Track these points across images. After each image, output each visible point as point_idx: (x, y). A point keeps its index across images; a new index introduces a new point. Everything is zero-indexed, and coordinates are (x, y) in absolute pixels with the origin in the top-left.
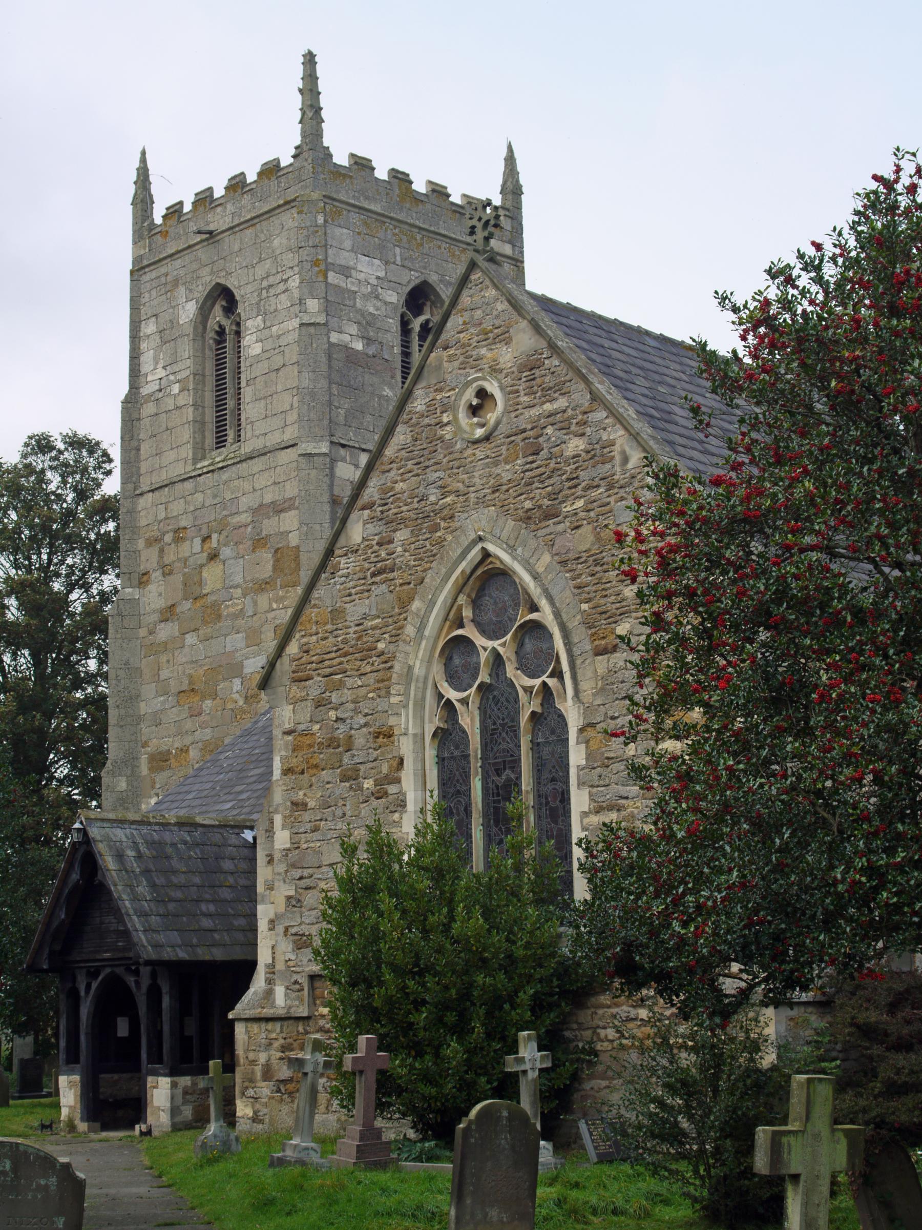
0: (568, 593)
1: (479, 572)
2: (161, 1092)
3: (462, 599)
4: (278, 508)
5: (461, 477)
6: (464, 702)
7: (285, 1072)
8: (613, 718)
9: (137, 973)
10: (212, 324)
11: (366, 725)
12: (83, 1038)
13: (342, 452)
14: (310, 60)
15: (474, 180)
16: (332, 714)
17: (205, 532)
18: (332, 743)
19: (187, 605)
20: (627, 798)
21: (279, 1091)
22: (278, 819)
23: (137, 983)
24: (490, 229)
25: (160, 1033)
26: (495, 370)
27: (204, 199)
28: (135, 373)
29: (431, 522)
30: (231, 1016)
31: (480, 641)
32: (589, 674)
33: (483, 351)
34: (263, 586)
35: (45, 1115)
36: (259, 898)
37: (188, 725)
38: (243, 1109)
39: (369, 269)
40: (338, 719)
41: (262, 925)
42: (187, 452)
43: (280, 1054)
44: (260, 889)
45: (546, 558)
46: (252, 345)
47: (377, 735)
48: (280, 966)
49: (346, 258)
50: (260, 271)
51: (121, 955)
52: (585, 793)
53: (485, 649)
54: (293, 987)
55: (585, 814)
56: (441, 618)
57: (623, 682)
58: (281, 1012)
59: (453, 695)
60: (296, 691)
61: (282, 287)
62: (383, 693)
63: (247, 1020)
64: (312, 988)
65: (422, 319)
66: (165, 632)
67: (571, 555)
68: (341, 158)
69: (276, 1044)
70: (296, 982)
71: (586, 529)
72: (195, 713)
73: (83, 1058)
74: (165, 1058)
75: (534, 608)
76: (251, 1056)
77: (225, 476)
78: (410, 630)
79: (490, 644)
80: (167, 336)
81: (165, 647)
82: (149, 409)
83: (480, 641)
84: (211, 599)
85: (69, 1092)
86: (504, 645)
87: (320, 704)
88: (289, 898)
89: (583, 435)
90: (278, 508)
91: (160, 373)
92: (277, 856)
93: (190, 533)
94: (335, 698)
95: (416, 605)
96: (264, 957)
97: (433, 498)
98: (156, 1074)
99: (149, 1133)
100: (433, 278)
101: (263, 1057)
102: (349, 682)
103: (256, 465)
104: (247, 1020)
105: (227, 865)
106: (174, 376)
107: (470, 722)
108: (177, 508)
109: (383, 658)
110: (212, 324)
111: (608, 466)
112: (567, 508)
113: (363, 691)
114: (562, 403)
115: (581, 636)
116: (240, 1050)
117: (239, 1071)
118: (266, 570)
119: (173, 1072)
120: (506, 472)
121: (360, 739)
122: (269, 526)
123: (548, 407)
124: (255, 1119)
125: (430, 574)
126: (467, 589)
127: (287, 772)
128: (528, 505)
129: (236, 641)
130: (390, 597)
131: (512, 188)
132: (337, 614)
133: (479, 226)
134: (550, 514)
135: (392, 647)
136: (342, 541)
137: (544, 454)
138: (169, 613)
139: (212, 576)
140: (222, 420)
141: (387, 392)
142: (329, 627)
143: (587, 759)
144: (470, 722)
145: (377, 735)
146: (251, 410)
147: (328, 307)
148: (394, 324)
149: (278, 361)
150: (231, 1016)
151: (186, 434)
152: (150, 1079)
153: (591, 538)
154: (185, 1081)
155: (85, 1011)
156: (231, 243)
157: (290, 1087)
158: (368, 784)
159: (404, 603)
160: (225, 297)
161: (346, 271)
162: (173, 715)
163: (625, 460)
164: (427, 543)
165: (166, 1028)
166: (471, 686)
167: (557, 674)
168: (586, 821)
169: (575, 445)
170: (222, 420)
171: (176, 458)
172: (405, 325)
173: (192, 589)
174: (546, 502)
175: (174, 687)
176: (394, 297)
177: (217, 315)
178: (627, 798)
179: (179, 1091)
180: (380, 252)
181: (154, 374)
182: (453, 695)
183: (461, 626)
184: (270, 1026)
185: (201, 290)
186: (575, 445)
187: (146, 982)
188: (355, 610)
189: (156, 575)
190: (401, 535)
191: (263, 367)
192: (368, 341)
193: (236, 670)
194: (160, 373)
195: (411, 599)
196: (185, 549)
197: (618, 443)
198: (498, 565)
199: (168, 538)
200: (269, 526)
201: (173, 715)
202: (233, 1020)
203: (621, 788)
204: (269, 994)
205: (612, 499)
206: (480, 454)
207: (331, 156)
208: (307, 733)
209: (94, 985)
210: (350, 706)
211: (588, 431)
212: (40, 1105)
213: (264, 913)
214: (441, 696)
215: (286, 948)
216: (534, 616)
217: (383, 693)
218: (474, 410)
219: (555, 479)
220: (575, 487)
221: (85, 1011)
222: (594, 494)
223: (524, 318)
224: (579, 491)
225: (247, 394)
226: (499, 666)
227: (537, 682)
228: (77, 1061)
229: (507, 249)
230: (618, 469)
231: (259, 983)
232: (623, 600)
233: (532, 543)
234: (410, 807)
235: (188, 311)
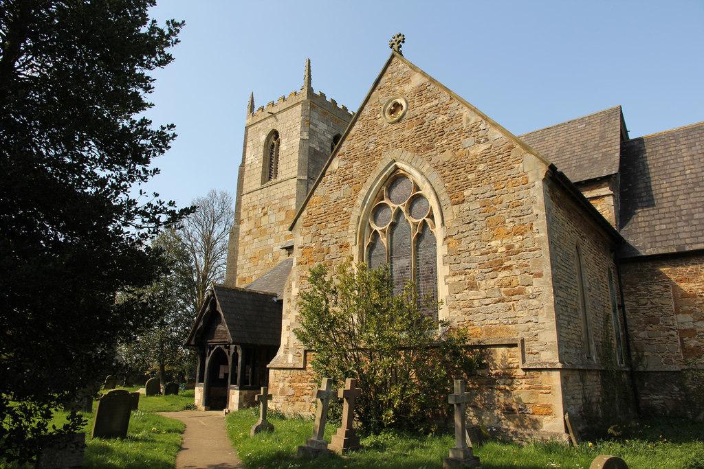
0: (438, 179)
1: (392, 176)
2: (235, 396)
3: (384, 189)
4: (288, 198)
5: (385, 138)
6: (383, 231)
7: (291, 392)
8: (462, 232)
9: (229, 348)
10: (271, 143)
11: (336, 242)
12: (206, 373)
16: (321, 239)
17: (263, 206)
18: (321, 251)
20: (470, 269)
21: (287, 400)
22: (294, 284)
23: (229, 352)
24: (401, 43)
25: (236, 375)
26: (402, 94)
30: (268, 366)
32: (450, 213)
35: (188, 401)
36: (283, 317)
39: (322, 127)
40: (323, 241)
43: (289, 384)
44: (284, 313)
45: (427, 166)
46: (283, 147)
47: (341, 247)
48: (291, 345)
49: (315, 121)
50: (288, 125)
51: (223, 340)
52: (447, 267)
53: (394, 208)
54: (297, 355)
55: (446, 277)
56: (374, 196)
57: (468, 216)
58: (291, 366)
62: (345, 229)
63: (275, 369)
64: (305, 356)
66: (248, 238)
67: (441, 163)
68: (317, 92)
69: (287, 379)
70: (298, 353)
73: (205, 380)
74: (238, 382)
76: (276, 384)
77: (271, 188)
79: (397, 206)
80: (254, 147)
84: (263, 228)
85: (199, 393)
88: (297, 316)
89: (446, 114)
90: (288, 198)
91: (252, 157)
92: (292, 299)
93: (258, 207)
96: (284, 341)
97: (372, 148)
98: (233, 389)
99: (229, 411)
101: (281, 385)
102: (329, 225)
104: (275, 369)
105: (267, 309)
106: (255, 158)
108: (254, 199)
109: (345, 215)
110: (271, 143)
111: (460, 124)
113: (336, 228)
114: (436, 102)
115: (444, 197)
116: (271, 381)
120: (407, 133)
121: (333, 249)
122: (286, 203)
123: (428, 105)
125: (369, 178)
126: (386, 184)
127: (299, 264)
128: (418, 145)
129: (271, 241)
130: (349, 189)
133: (396, 43)
135: (350, 210)
136: (329, 170)
137: (426, 124)
140: (270, 170)
142: (322, 204)
143: (448, 251)
145: (341, 247)
147: (310, 135)
148: (329, 145)
149: (291, 151)
150: (268, 366)
151: (259, 176)
152: (231, 391)
153: (451, 155)
154: (245, 392)
155: (207, 362)
156: (279, 116)
157: (292, 399)
160: (275, 134)
161: (316, 126)
162: (248, 265)
163: (468, 120)
164: (368, 166)
166: (385, 225)
167: (431, 216)
168: (447, 280)
170: (270, 170)
171: (254, 178)
173: (258, 225)
174: (427, 143)
175: (249, 256)
178: (470, 269)
179: (243, 396)
180: (326, 122)
183: (383, 199)
184: (285, 371)
186: (442, 118)
187: (232, 351)
188: (334, 196)
190: (357, 163)
191: (286, 154)
192: (321, 148)
193: (270, 250)
194: (252, 157)
195: (360, 189)
196: (256, 212)
197: (465, 115)
198: (402, 172)
199: (251, 209)
201: (248, 265)
202: (269, 368)
203: (466, 264)
204: (286, 357)
205: (461, 138)
206: (394, 128)
209: (212, 352)
210: (330, 235)
211: (449, 111)
212: (542, 393)
213: (285, 323)
214: (371, 229)
215: (294, 338)
217: (345, 229)
218: (392, 112)
219: (432, 133)
220: (442, 135)
221: (207, 362)
222: (451, 137)
223: (417, 72)
224: (444, 136)
225: (280, 162)
228: (203, 382)
230: (464, 125)
231: (280, 353)
232: (468, 180)
233: (420, 160)
235: (263, 138)
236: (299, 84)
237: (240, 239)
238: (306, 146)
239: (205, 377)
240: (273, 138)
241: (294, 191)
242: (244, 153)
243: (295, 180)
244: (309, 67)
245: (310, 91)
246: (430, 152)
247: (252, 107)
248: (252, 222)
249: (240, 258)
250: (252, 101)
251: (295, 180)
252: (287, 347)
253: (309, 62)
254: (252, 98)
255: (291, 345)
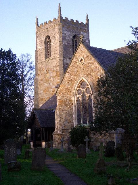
4: (56, 66)
13: (65, 59)
14: (60, 5)
15: (82, 20)
19: (44, 79)
22: (58, 110)
27: (46, 23)
28: (37, 47)
29: (76, 75)
31: (82, 89)
33: (82, 54)
34: (55, 77)
37: (45, 95)
38: (54, 146)
39: (68, 33)
41: (56, 123)
42: (44, 58)
46: (52, 44)
48: (58, 128)
54: (60, 131)
59: (79, 96)
60: (60, 95)
61: (56, 36)
65: (75, 39)
66: (41, 82)
68: (64, 18)
71: (94, 77)
72: (46, 94)
75: (88, 86)
78: (73, 88)
79: (83, 90)
80: (41, 42)
81: (41, 84)
82: (39, 52)
83: (82, 89)
86: (84, 90)
87: (63, 96)
90: (56, 66)
91: (40, 47)
94: (65, 96)
95: (74, 85)
96: (56, 127)
100: (77, 34)
103: (54, 60)
106: (42, 47)
107: (80, 99)
108: (43, 66)
112: (92, 74)
117: (53, 141)
118: (55, 75)
119: (45, 141)
122: (55, 69)
124: (56, 147)
128: (87, 73)
131: (88, 20)
132: (65, 85)
134: (90, 74)
138: (42, 80)
139: (48, 75)
140: (48, 54)
141: (71, 50)
144: (80, 99)
146: (52, 53)
148: (71, 41)
151: (44, 56)
158: (69, 106)
159: (73, 84)
160: (48, 37)
161: (65, 34)
165: (44, 137)
169: (93, 66)
170: (48, 54)
171: (42, 58)
172: (73, 40)
173: (45, 77)
176: (71, 37)
177: (48, 40)
180: (70, 31)
181: (39, 47)
182: (79, 96)
185: (46, 36)
186: (93, 66)
187: (41, 130)
189: (40, 75)
192: (68, 43)
193: (51, 88)
194: (40, 47)
200: (55, 69)
207: (62, 18)
208: (61, 100)
213: (56, 122)
214: (77, 96)
215: (59, 126)
216: (88, 87)
226: (79, 120)
227: (88, 95)
229: (87, 29)
231: (56, 130)
234: (74, 109)
235: (44, 39)
236: (56, 16)
237: (38, 82)
238: (62, 44)
239: (44, 138)
240: (48, 39)
241: (58, 64)
242: (36, 45)
243: (58, 59)
244: (60, 9)
245: (61, 17)
246: (90, 76)
247: (37, 23)
248: (43, 75)
249: (39, 90)
250: (37, 20)
251: (58, 59)
252: (57, 129)
253: (60, 5)
254: (37, 19)
255: (58, 128)
